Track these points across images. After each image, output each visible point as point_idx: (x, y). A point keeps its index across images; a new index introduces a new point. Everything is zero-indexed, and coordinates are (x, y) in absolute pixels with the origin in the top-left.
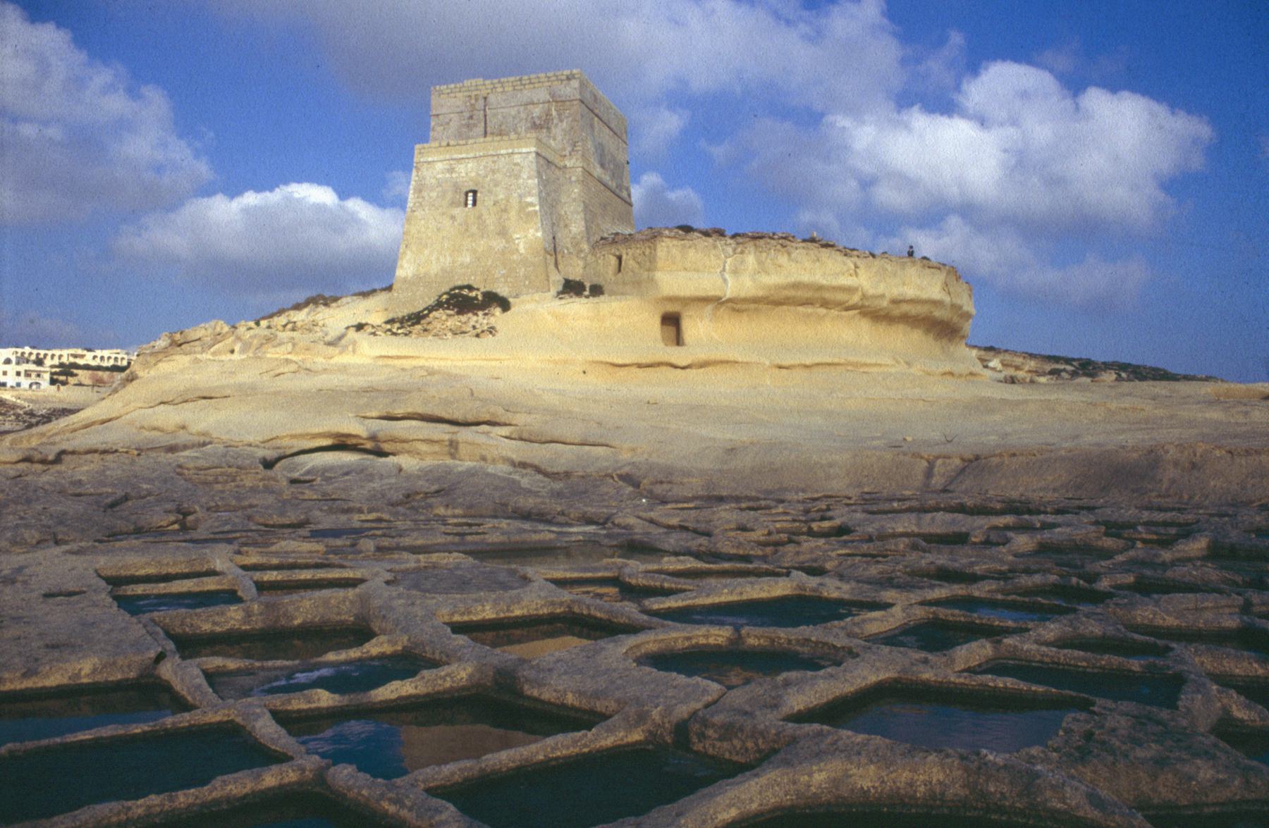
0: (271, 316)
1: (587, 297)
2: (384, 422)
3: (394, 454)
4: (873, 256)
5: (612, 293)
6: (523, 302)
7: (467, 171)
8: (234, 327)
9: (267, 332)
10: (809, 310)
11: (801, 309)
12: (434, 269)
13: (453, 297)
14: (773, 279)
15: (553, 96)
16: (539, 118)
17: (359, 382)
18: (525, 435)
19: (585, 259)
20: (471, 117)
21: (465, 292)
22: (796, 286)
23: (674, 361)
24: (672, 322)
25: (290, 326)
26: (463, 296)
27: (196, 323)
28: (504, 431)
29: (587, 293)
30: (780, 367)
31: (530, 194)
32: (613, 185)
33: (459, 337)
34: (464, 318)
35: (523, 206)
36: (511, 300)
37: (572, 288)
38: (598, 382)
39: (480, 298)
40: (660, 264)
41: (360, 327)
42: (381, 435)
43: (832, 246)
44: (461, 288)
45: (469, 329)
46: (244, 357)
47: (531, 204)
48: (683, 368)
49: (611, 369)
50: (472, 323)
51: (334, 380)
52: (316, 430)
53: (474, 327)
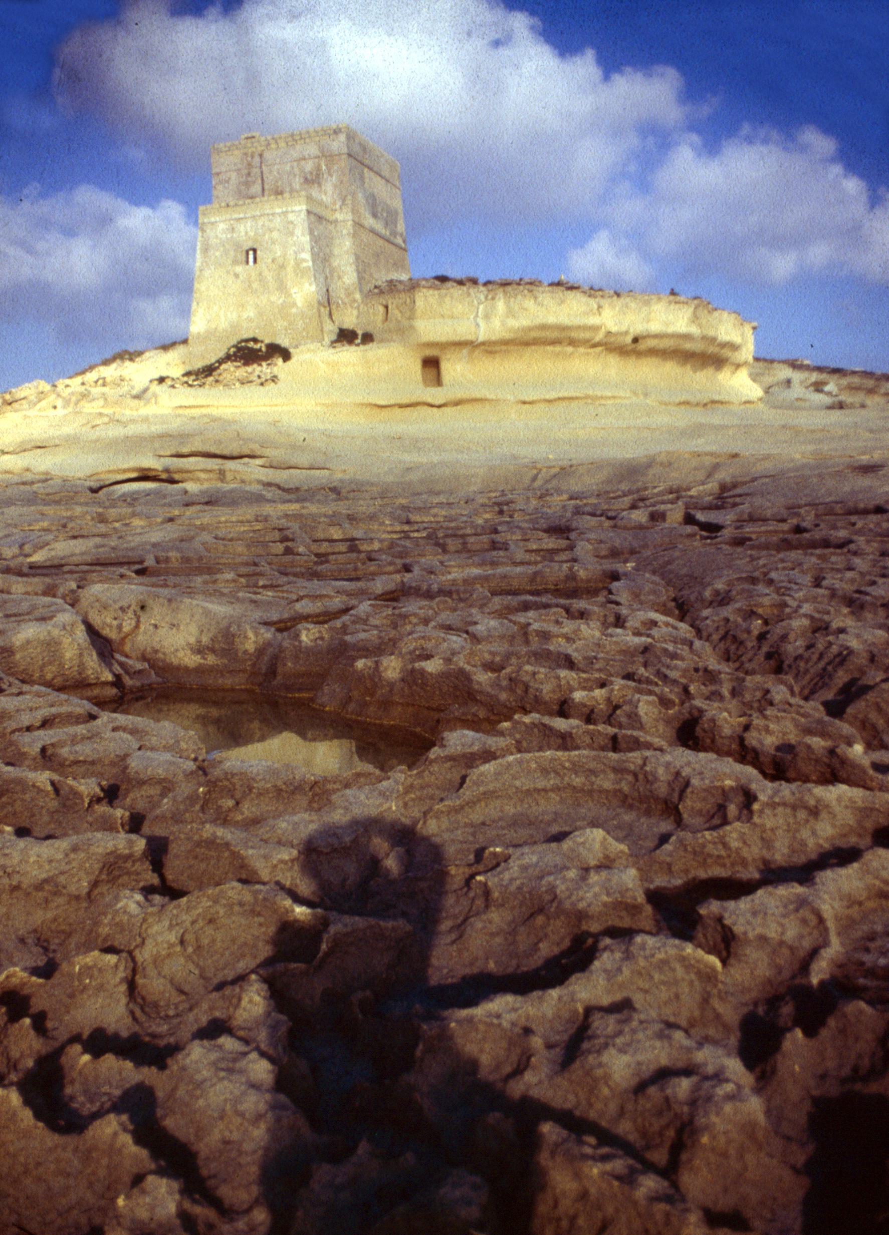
0: (83, 372)
1: (358, 345)
2: (175, 459)
3: (182, 482)
4: (618, 295)
5: (382, 341)
6: (302, 352)
7: (246, 231)
8: (55, 386)
9: (82, 389)
10: (558, 348)
11: (550, 348)
12: (223, 324)
13: (239, 349)
14: (522, 322)
15: (322, 152)
16: (311, 173)
17: (156, 429)
18: (274, 464)
19: (358, 308)
20: (249, 174)
21: (251, 345)
22: (543, 327)
23: (430, 400)
24: (431, 364)
25: (101, 382)
26: (248, 348)
27: (17, 384)
28: (258, 462)
29: (358, 341)
30: (524, 403)
31: (303, 250)
32: (386, 232)
33: (246, 387)
34: (249, 369)
35: (298, 263)
36: (291, 350)
37: (346, 336)
38: (361, 424)
39: (264, 349)
40: (419, 312)
41: (162, 380)
42: (172, 468)
43: (577, 288)
44: (247, 341)
45: (255, 378)
46: (66, 411)
47: (304, 260)
48: (439, 406)
49: (376, 411)
50: (257, 373)
51: (133, 430)
52: (126, 466)
53: (259, 377)
